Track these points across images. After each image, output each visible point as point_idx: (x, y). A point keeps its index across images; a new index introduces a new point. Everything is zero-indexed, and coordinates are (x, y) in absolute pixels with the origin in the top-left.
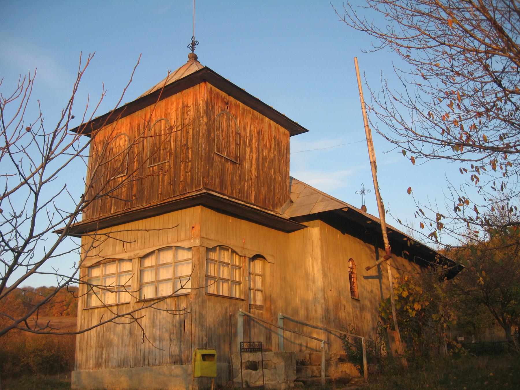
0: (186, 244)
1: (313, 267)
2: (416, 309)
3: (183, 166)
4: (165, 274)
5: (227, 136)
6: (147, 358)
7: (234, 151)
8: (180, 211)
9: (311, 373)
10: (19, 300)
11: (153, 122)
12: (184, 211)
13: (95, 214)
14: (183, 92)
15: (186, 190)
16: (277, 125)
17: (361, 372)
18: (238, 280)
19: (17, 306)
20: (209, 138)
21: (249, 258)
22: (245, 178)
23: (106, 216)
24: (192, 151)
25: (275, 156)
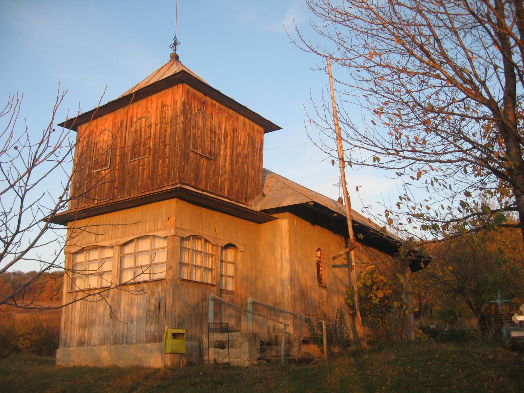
0: (162, 234)
1: (281, 256)
2: (379, 296)
3: (161, 161)
4: (144, 260)
5: (203, 133)
6: (125, 337)
7: (209, 148)
8: (157, 203)
9: (275, 353)
10: (9, 284)
11: (135, 120)
12: (161, 202)
13: (80, 204)
14: (162, 92)
15: (163, 184)
16: (252, 123)
17: (322, 351)
18: (210, 267)
19: (6, 291)
20: (185, 136)
21: (221, 247)
22: (219, 173)
23: (90, 206)
24: (170, 148)
25: (248, 152)
